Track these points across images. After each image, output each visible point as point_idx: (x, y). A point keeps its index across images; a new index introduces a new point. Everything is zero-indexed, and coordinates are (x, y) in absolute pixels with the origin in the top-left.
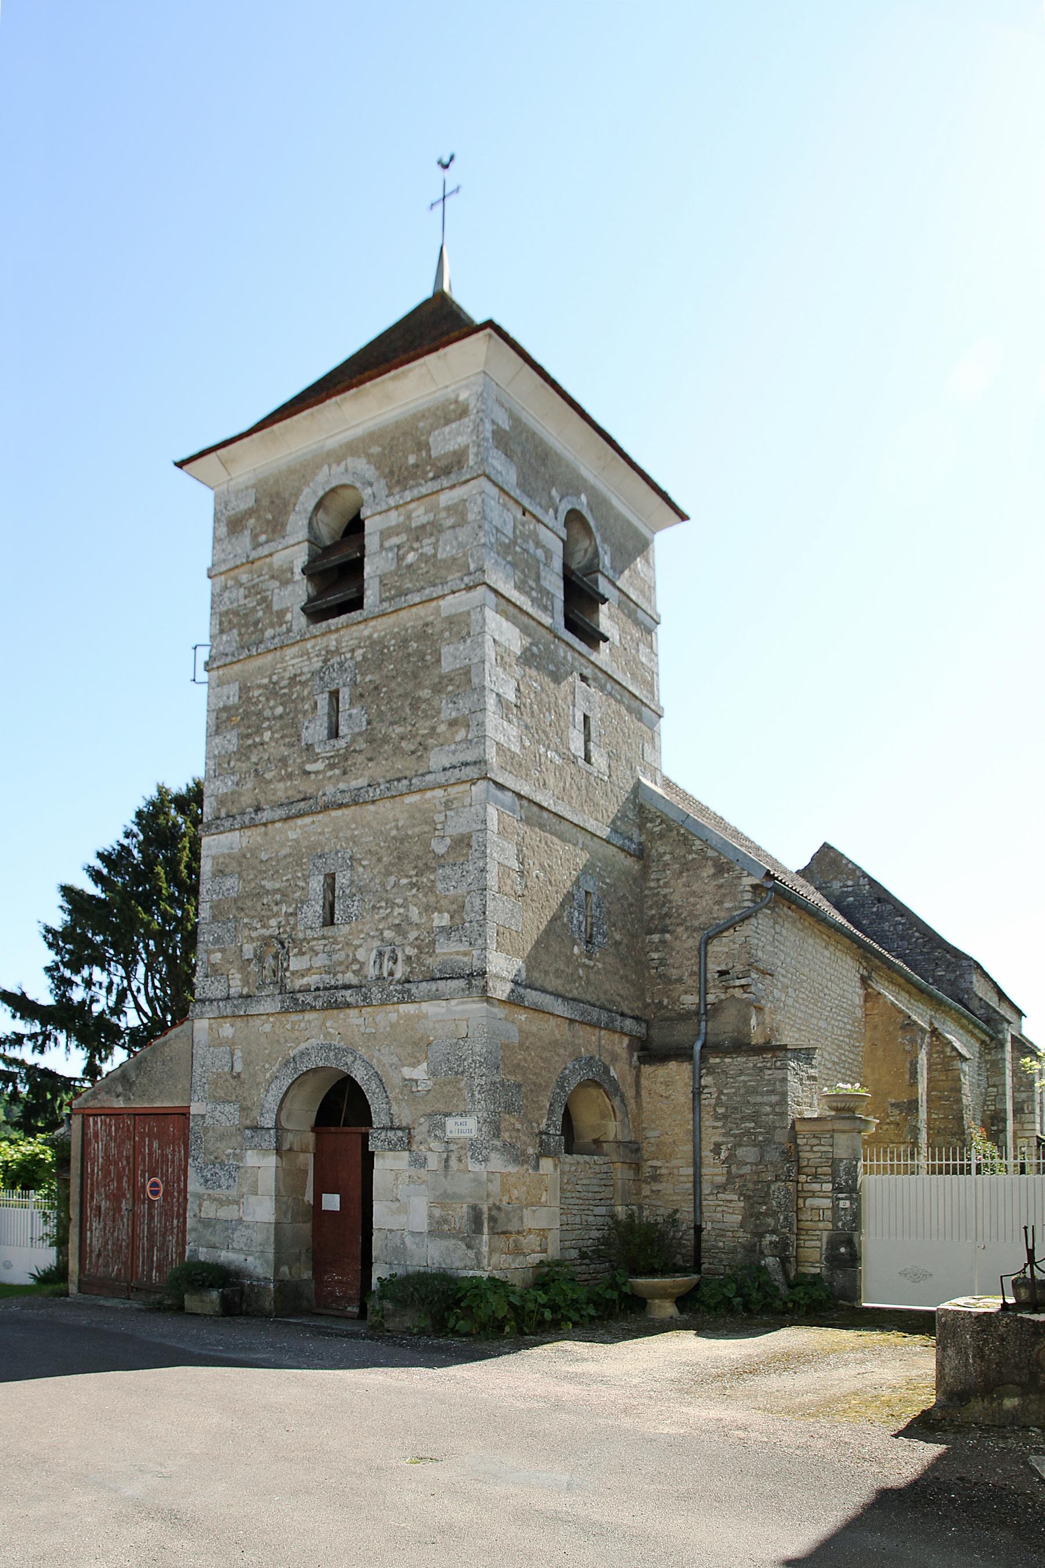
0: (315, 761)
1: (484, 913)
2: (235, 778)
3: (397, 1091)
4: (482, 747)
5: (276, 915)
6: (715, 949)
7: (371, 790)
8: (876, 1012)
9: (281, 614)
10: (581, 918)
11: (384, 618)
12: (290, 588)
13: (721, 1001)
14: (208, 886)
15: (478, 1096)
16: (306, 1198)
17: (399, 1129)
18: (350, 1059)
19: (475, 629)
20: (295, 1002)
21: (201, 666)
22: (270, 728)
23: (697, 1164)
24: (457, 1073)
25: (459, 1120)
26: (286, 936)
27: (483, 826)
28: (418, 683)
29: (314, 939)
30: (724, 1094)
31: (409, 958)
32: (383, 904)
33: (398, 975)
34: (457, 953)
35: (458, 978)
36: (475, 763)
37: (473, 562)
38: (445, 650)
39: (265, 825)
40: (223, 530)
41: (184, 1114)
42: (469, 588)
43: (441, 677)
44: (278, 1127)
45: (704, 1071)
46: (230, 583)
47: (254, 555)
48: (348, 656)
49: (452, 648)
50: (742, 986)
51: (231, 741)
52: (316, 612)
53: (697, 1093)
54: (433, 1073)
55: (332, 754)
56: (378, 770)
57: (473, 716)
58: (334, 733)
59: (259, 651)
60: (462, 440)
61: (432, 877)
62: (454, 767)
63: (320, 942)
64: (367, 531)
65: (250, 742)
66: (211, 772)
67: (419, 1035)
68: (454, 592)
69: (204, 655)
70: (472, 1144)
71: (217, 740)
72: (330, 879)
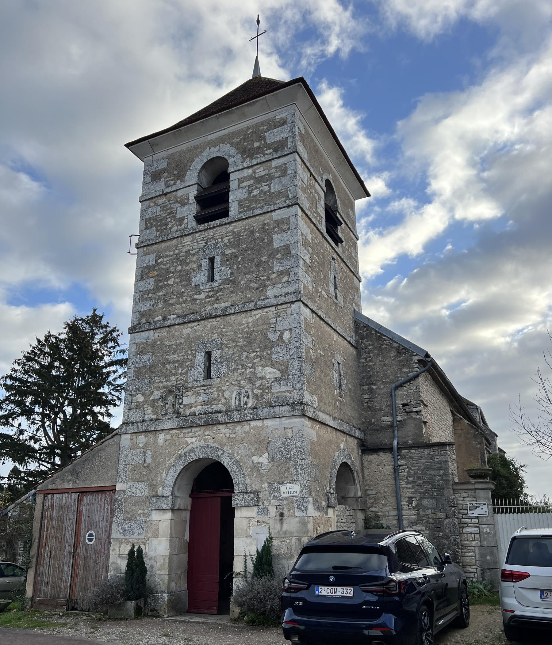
0: (200, 294)
1: (300, 370)
2: (152, 303)
3: (250, 470)
4: (297, 285)
5: (175, 374)
7: (233, 308)
9: (182, 219)
10: (337, 376)
11: (240, 222)
12: (186, 207)
13: (405, 420)
14: (133, 360)
15: (300, 471)
16: (185, 538)
18: (220, 453)
19: (292, 226)
20: (188, 423)
21: (133, 245)
22: (173, 277)
23: (399, 508)
24: (287, 458)
25: (288, 486)
26: (181, 386)
27: (299, 325)
28: (259, 254)
29: (198, 387)
30: (412, 470)
31: (256, 395)
32: (240, 367)
33: (249, 405)
34: (285, 392)
36: (294, 293)
38: (275, 237)
40: (149, 179)
41: (111, 490)
42: (289, 206)
43: (274, 250)
44: (173, 495)
45: (399, 457)
47: (167, 190)
48: (220, 240)
49: (279, 236)
50: (417, 412)
51: (150, 284)
52: (200, 219)
53: (396, 469)
54: (272, 459)
56: (237, 298)
57: (292, 269)
58: (211, 279)
59: (169, 238)
60: (284, 135)
61: (269, 352)
62: (281, 295)
63: (202, 388)
64: (231, 179)
65: (161, 284)
66: (137, 300)
67: (262, 437)
68: (280, 208)
69: (136, 240)
70: (297, 500)
71: (141, 283)
72: (209, 355)
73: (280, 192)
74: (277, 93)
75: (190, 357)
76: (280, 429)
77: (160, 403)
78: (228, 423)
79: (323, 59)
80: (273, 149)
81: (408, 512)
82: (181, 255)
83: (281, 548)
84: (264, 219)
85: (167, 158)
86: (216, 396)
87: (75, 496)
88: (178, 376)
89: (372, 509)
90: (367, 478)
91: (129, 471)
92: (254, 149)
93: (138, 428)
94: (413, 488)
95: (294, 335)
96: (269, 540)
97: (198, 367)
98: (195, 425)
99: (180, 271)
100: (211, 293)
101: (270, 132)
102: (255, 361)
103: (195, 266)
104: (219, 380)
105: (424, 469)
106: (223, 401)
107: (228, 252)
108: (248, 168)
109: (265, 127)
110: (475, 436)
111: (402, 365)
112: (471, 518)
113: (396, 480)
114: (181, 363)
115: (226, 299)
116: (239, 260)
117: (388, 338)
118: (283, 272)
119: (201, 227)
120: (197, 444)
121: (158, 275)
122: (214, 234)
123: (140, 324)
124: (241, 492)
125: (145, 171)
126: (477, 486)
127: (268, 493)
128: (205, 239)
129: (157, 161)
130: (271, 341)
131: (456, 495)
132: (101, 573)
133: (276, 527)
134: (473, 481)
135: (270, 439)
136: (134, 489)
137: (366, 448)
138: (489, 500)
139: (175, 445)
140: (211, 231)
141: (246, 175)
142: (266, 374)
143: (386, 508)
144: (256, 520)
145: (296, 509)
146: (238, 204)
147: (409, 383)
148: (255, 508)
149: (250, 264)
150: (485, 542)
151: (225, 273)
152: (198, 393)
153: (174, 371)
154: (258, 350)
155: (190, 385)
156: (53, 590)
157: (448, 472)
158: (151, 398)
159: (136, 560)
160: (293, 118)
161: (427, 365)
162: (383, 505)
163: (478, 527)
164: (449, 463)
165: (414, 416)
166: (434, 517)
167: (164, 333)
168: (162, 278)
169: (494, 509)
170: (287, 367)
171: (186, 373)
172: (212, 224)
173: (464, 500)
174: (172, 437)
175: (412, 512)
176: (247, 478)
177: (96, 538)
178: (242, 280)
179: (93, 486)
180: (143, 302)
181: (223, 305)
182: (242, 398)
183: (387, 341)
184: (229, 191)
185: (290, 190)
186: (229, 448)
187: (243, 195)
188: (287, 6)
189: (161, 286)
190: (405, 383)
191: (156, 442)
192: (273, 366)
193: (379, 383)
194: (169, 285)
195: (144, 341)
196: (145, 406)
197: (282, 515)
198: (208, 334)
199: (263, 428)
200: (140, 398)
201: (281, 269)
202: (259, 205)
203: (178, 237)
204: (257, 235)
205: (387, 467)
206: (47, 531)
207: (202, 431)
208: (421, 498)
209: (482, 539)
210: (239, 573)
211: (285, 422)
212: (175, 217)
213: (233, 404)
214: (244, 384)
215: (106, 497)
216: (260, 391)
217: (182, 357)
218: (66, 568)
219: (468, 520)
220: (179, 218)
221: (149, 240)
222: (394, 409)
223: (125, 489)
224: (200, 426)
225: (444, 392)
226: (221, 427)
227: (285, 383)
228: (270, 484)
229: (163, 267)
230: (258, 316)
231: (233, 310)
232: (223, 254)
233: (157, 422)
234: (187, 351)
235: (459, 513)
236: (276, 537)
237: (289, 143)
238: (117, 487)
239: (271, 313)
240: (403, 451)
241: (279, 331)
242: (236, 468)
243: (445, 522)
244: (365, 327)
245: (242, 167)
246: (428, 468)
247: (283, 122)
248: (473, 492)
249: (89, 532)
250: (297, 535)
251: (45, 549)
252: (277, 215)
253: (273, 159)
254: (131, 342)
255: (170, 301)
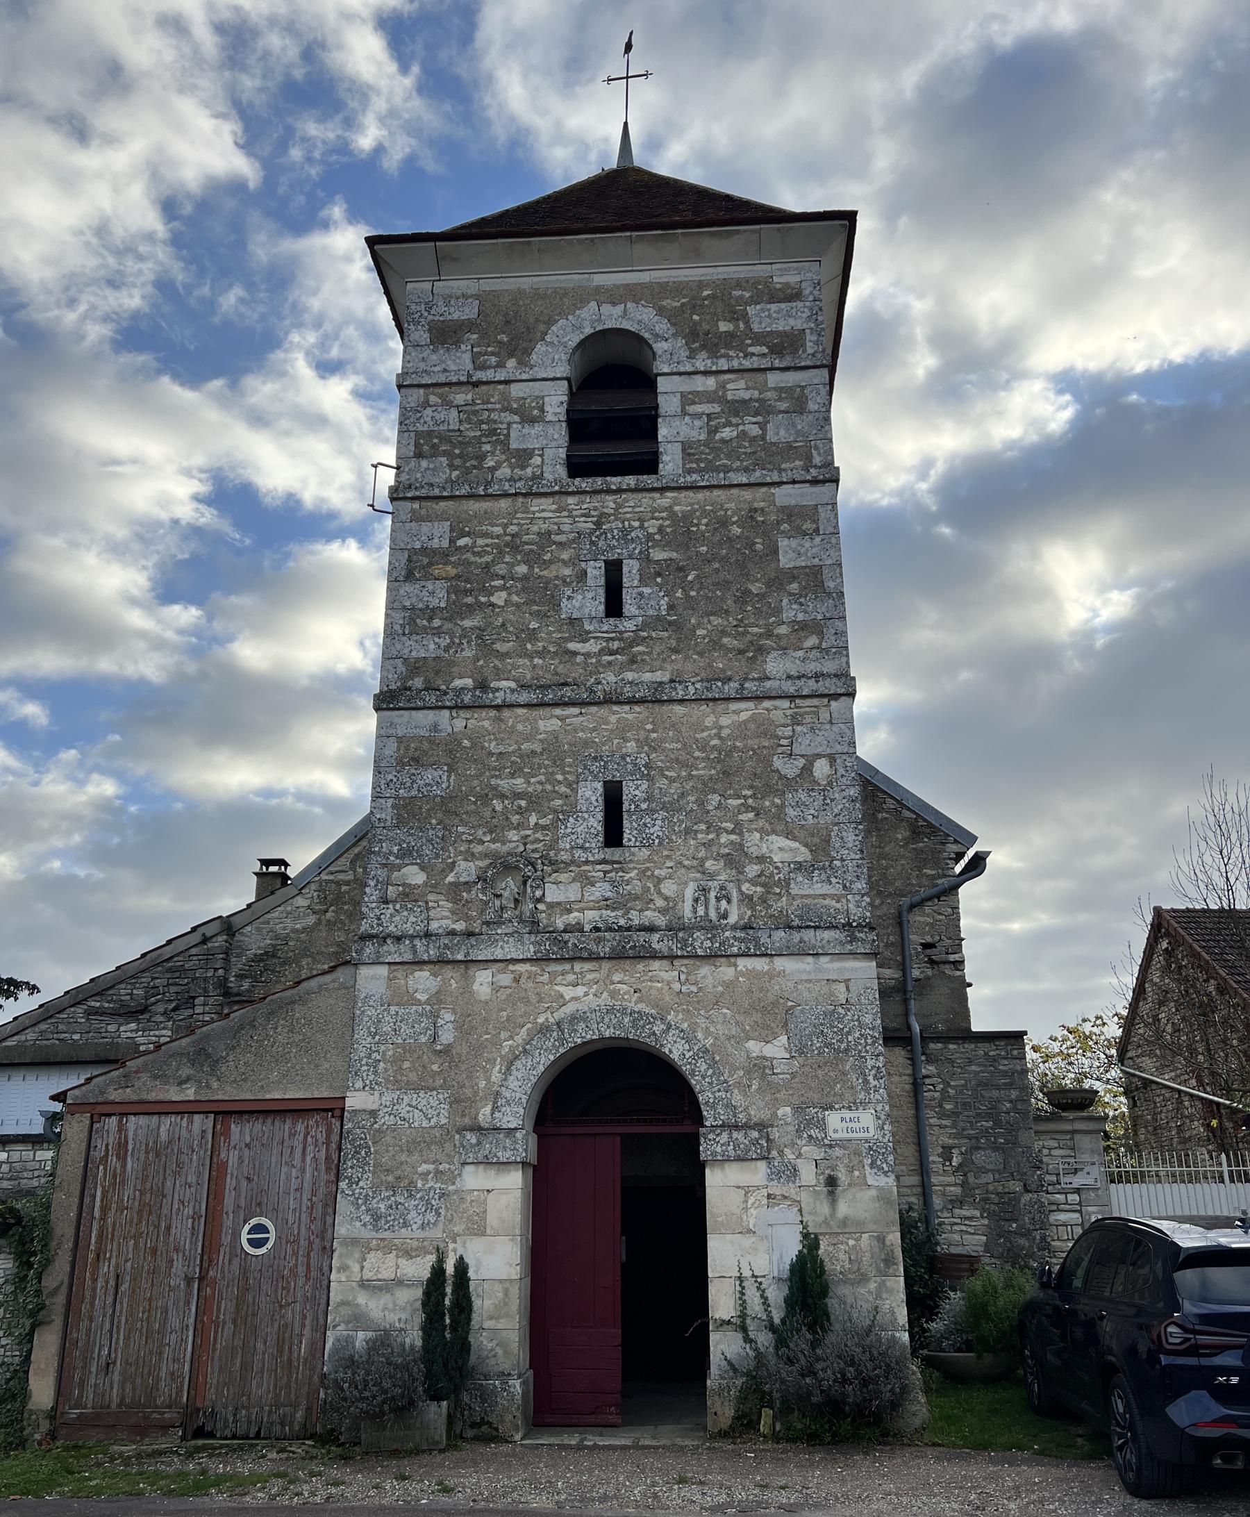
0: (585, 641)
2: (444, 641)
4: (844, 659)
9: (529, 453)
11: (690, 494)
12: (538, 428)
13: (928, 978)
14: (390, 777)
15: (873, 1083)
18: (659, 1028)
20: (563, 948)
22: (504, 588)
24: (838, 1051)
25: (847, 1114)
29: (587, 862)
31: (750, 898)
32: (703, 827)
33: (732, 919)
34: (824, 896)
35: (828, 928)
36: (836, 675)
37: (819, 454)
38: (783, 543)
39: (498, 707)
41: (334, 1109)
43: (782, 571)
50: (954, 963)
54: (800, 1050)
57: (828, 623)
59: (490, 491)
60: (799, 324)
61: (777, 801)
63: (599, 867)
65: (469, 600)
67: (771, 998)
68: (794, 482)
71: (408, 587)
73: (790, 446)
74: (789, 229)
75: (563, 789)
76: (818, 981)
77: (477, 894)
78: (677, 957)
79: (344, 159)
80: (768, 347)
81: (942, 1178)
82: (525, 538)
84: (755, 497)
86: (638, 890)
87: (201, 1123)
88: (529, 832)
91: (385, 1061)
92: (720, 336)
94: (954, 1126)
95: (841, 771)
96: (811, 1242)
97: (586, 816)
98: (586, 955)
99: (525, 578)
100: (616, 645)
101: (758, 307)
102: (740, 817)
103: (567, 572)
104: (645, 852)
106: (660, 903)
107: (658, 555)
108: (706, 373)
109: (747, 295)
111: (921, 860)
114: (535, 802)
115: (655, 663)
116: (690, 578)
118: (806, 625)
120: (590, 1002)
121: (458, 577)
124: (722, 1126)
128: (593, 513)
129: (448, 299)
132: (297, 1330)
135: (790, 1004)
136: (403, 1109)
139: (526, 1001)
140: (610, 498)
141: (700, 389)
142: (771, 851)
148: (762, 1166)
152: (587, 878)
153: (515, 819)
154: (749, 793)
155: (564, 856)
156: (129, 1387)
158: (450, 878)
159: (447, 1298)
160: (816, 293)
163: (1080, 1212)
165: (948, 970)
166: (1000, 1189)
167: (483, 721)
168: (469, 586)
170: (827, 841)
171: (554, 826)
172: (615, 482)
175: (951, 1179)
177: (278, 1238)
178: (699, 625)
179: (268, 1096)
180: (414, 637)
181: (647, 677)
182: (713, 901)
183: (890, 804)
184: (656, 416)
186: (681, 1016)
188: (273, 21)
189: (468, 605)
190: (930, 899)
191: (467, 989)
192: (789, 835)
194: (493, 605)
196: (431, 897)
197: (832, 1182)
198: (610, 740)
199: (771, 975)
201: (800, 617)
202: (738, 463)
203: (516, 494)
204: (736, 530)
206: (103, 1218)
207: (604, 971)
210: (729, 1322)
211: (830, 966)
213: (688, 912)
214: (714, 868)
215: (316, 1129)
216: (759, 889)
217: (540, 788)
218: (174, 1321)
219: (1060, 1197)
220: (518, 450)
223: (375, 1107)
224: (599, 958)
226: (656, 965)
227: (824, 877)
228: (798, 1110)
229: (473, 559)
230: (744, 716)
231: (681, 693)
232: (645, 559)
233: (473, 940)
234: (552, 773)
238: (349, 1103)
240: (932, 1046)
241: (802, 756)
242: (704, 1066)
243: (1023, 1201)
246: (986, 1085)
248: (1068, 1137)
249: (254, 1221)
250: (874, 1228)
251: (96, 1268)
252: (786, 496)
253: (771, 369)
254: (383, 732)
255: (498, 646)
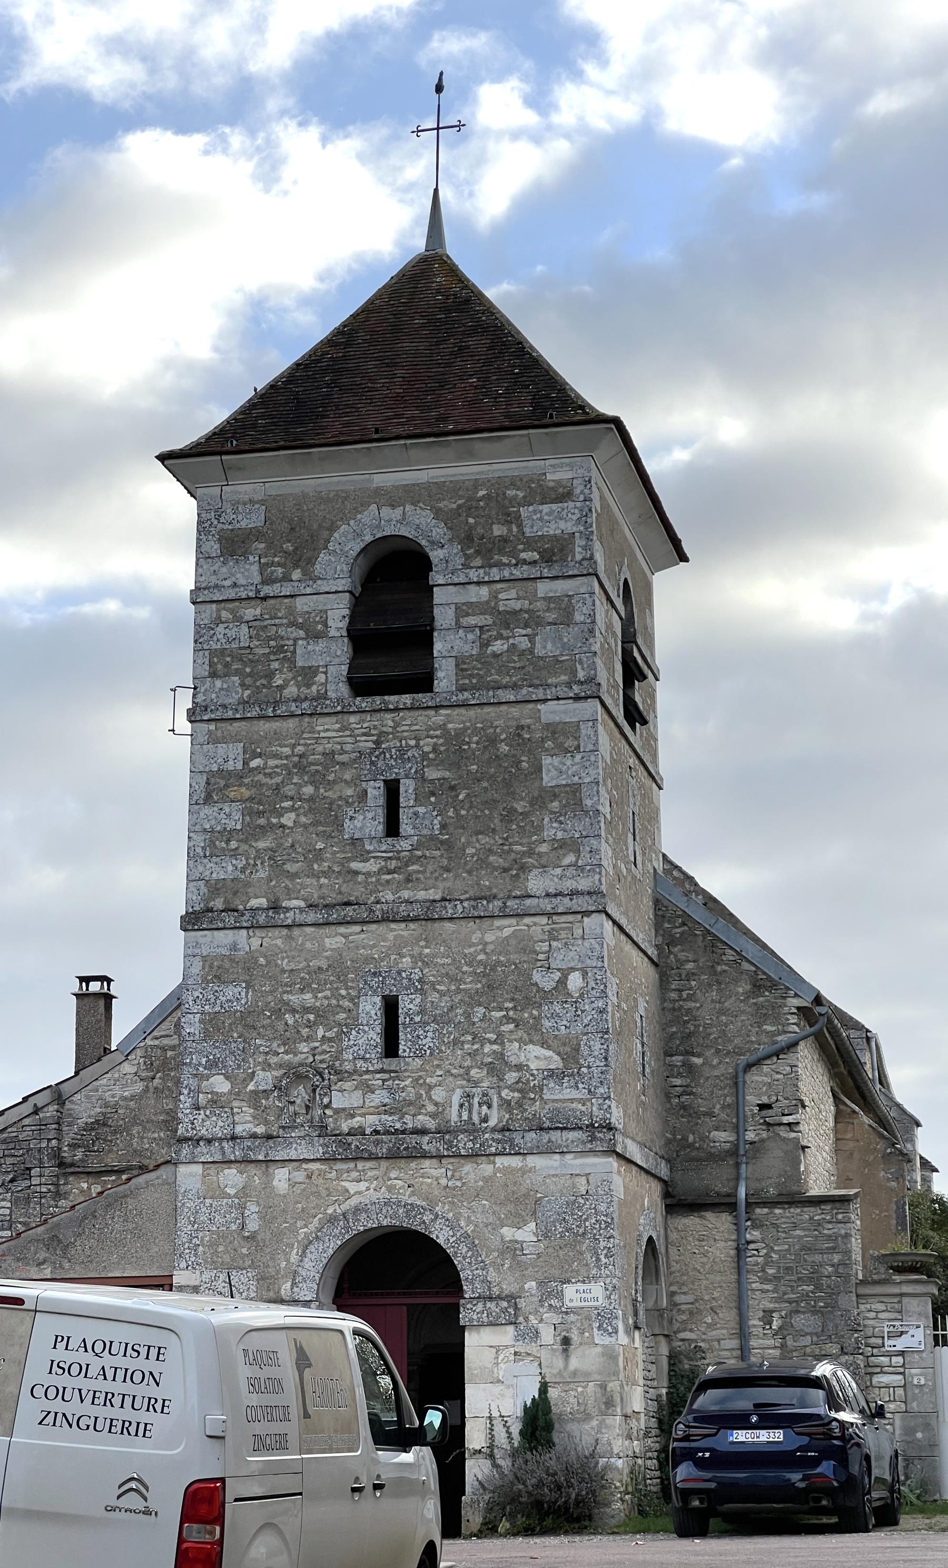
1: (606, 1059)
3: (496, 1254)
4: (597, 877)
5: (308, 1039)
6: (756, 1078)
8: (849, 1136)
11: (462, 711)
12: (321, 645)
13: (763, 1141)
14: (196, 994)
15: (604, 1260)
17: (499, 1298)
18: (427, 1217)
20: (347, 1149)
22: (292, 809)
23: (743, 1334)
24: (576, 1235)
25: (581, 1287)
27: (600, 964)
31: (509, 1103)
32: (469, 1038)
33: (492, 1122)
35: (574, 1129)
36: (589, 893)
38: (547, 761)
40: (213, 547)
43: (542, 789)
45: (749, 1223)
46: (225, 615)
47: (267, 590)
49: (556, 761)
50: (789, 1124)
51: (232, 817)
53: (740, 1251)
55: (390, 855)
59: (279, 712)
60: (568, 526)
61: (535, 1012)
63: (378, 1076)
65: (262, 821)
66: (199, 850)
67: (523, 1190)
68: (558, 699)
70: (599, 1314)
71: (207, 810)
75: (346, 1004)
76: (563, 1175)
77: (273, 1101)
78: (444, 1156)
81: (761, 1341)
83: (565, 1402)
85: (262, 502)
86: (412, 1097)
89: (682, 1335)
90: (675, 1267)
91: (203, 1245)
93: (224, 1153)
94: (775, 1291)
97: (366, 1028)
98: (366, 1155)
99: (311, 799)
100: (393, 864)
101: (531, 508)
102: (503, 1028)
103: (350, 792)
105: (801, 1250)
106: (431, 1108)
107: (432, 774)
109: (521, 494)
110: (886, 1157)
112: (890, 1355)
113: (739, 1274)
114: (322, 1015)
115: (431, 882)
116: (461, 797)
117: (732, 948)
118: (564, 843)
119: (364, 703)
120: (371, 1196)
121: (251, 799)
122: (397, 725)
123: (211, 910)
125: (199, 523)
126: (906, 1289)
127: (536, 1299)
128: (373, 732)
130: (540, 990)
131: (862, 1307)
133: (554, 1364)
134: (897, 1278)
135: (539, 1195)
137: (677, 1203)
138: (927, 1317)
139: (317, 1194)
140: (388, 716)
141: (474, 600)
143: (714, 1333)
144: (512, 1350)
145: (595, 1330)
146: (457, 666)
147: (775, 1058)
148: (511, 1329)
149: (487, 812)
150: (915, 1405)
151: (427, 822)
152: (368, 1086)
153: (305, 1032)
154: (510, 1005)
155: (348, 1067)
157: (850, 1258)
158: (251, 1087)
161: (816, 1022)
162: (709, 1326)
163: (903, 1374)
164: (853, 1240)
165: (783, 1132)
167: (276, 939)
169: (936, 1337)
170: (577, 1049)
171: (338, 1038)
173: (876, 1316)
174: (309, 1177)
175: (771, 1342)
176: (491, 1269)
178: (469, 843)
179: (110, 1275)
180: (214, 859)
184: (432, 630)
185: (581, 662)
186: (447, 1207)
187: (467, 647)
190: (769, 1057)
192: (544, 1044)
193: (709, 1053)
194: (283, 826)
195: (225, 952)
197: (566, 1341)
198: (388, 956)
199: (524, 1171)
200: (221, 1085)
201: (560, 835)
202: (508, 679)
204: (504, 748)
205: (721, 1244)
207: (383, 1169)
208: (791, 1312)
209: (909, 1397)
212: (292, 662)
213: (454, 1117)
214: (478, 1076)
216: (516, 1094)
220: (303, 668)
221: (224, 706)
222: (741, 1116)
223: (197, 1283)
224: (377, 1158)
225: (827, 1056)
226: (427, 1163)
227: (572, 1083)
228: (541, 1284)
230: (507, 932)
233: (271, 1143)
234: (337, 989)
235: (867, 1345)
236: (555, 1383)
237: (578, 549)
239: (539, 928)
240: (758, 1211)
241: (558, 970)
242: (465, 1249)
244: (679, 916)
245: (466, 580)
246: (810, 1249)
247: (563, 495)
252: (551, 712)
255: (288, 867)
